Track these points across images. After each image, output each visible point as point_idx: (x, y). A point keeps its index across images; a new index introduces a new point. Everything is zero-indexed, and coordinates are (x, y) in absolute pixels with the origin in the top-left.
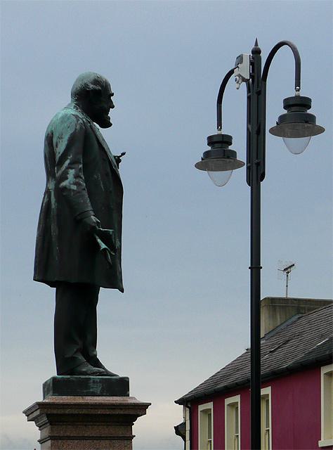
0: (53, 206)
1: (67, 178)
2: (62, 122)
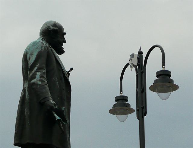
0: (27, 97)
1: (36, 78)
2: (33, 45)
